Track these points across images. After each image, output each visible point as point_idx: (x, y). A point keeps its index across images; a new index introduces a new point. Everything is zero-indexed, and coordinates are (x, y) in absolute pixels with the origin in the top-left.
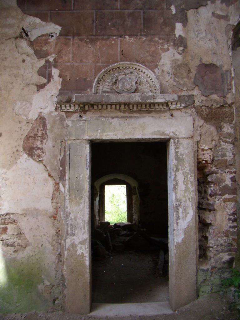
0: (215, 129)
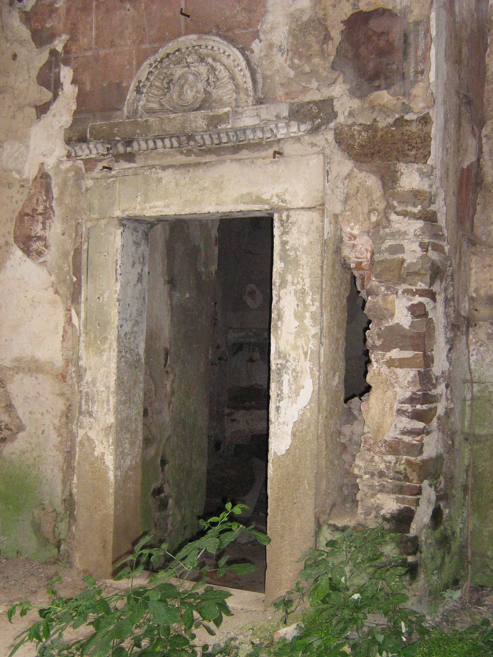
0: (380, 183)
